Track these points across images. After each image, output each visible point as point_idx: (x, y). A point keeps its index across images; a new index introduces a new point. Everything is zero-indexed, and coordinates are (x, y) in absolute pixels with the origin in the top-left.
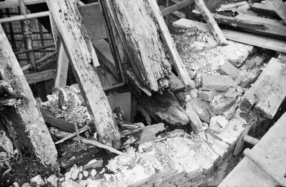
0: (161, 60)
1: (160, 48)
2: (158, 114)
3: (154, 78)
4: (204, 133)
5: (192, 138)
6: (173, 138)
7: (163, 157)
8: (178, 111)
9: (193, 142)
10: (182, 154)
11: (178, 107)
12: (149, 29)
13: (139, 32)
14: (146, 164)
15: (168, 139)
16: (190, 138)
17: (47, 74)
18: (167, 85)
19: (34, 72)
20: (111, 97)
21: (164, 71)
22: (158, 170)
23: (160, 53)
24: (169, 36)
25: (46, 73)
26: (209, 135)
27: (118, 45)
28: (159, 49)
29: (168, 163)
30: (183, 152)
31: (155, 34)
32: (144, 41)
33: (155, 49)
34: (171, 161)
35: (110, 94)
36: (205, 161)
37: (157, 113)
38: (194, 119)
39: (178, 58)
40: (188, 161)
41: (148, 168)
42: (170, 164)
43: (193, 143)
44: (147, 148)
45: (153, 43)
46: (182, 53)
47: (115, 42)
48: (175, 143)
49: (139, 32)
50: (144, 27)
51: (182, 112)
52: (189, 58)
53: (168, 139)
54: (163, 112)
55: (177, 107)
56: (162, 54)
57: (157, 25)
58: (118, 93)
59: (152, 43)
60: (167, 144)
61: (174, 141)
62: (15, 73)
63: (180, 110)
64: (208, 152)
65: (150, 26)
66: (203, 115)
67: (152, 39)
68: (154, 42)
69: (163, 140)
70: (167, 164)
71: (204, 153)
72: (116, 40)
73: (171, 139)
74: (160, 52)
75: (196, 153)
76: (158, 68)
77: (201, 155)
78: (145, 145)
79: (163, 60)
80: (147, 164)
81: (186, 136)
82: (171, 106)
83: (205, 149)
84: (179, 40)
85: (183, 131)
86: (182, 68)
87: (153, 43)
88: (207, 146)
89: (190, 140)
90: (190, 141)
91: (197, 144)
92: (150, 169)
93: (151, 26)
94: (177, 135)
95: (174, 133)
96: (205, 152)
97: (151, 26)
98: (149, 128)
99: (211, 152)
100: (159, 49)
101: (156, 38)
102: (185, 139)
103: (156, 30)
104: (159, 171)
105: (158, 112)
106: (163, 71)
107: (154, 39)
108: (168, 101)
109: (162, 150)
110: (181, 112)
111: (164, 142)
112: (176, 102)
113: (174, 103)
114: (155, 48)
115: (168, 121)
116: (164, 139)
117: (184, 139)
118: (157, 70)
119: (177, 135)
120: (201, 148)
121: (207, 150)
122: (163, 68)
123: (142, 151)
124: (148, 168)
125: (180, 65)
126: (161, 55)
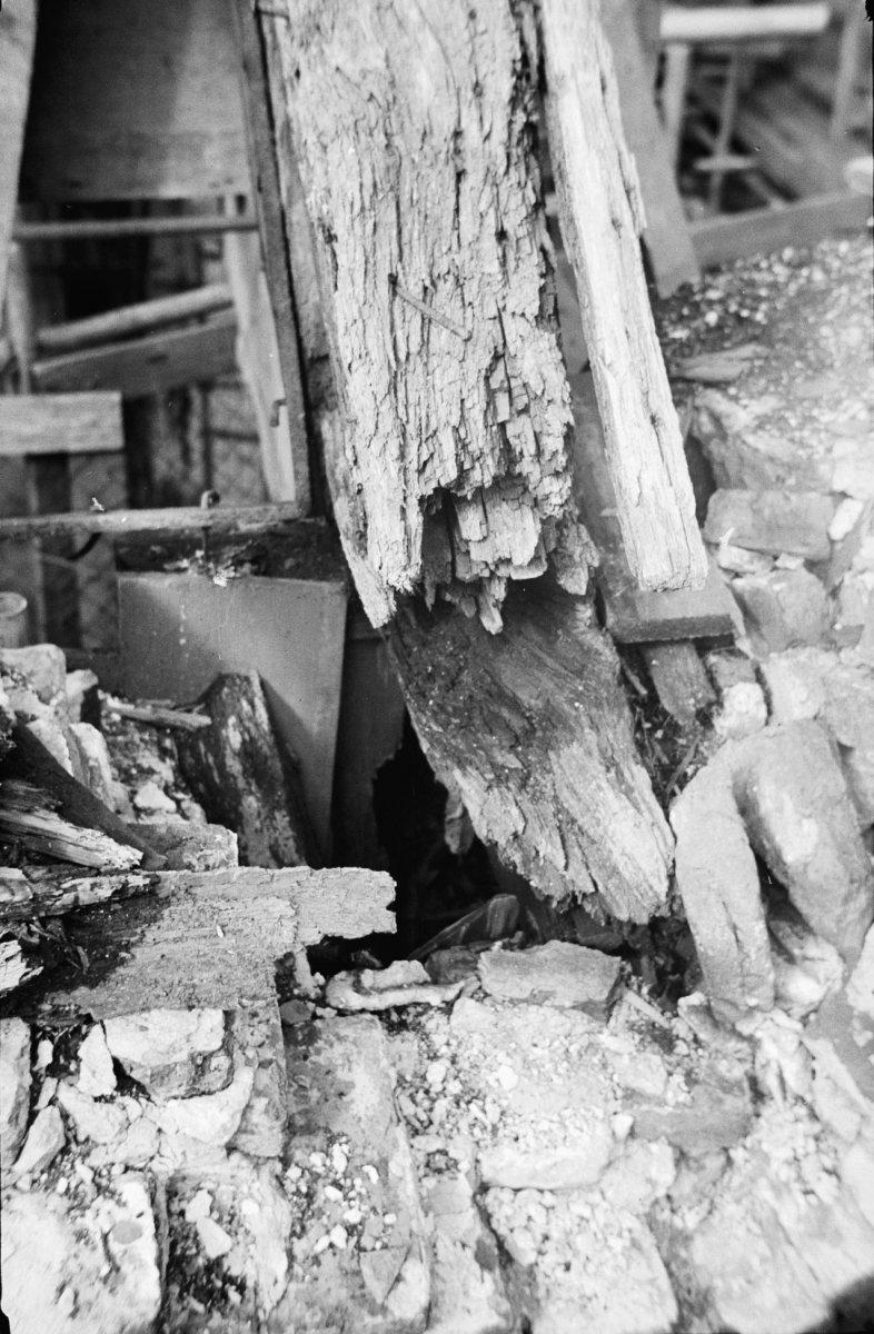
0: (494, 328)
1: (507, 227)
2: (463, 783)
3: (394, 467)
4: (799, 1026)
5: (681, 1048)
6: (508, 1013)
7: (340, 1164)
8: (611, 798)
9: (678, 1079)
10: (539, 1167)
11: (616, 765)
12: (449, 42)
13: (354, 55)
14: (110, 1204)
15: (467, 1009)
16: (666, 1041)
17: (87, 417)
18: (517, 561)
19: (17, 391)
20: (185, 587)
21: (511, 430)
22: (228, 1280)
23: (495, 267)
24: (602, 124)
25: (80, 407)
26: (835, 1058)
27: (290, 203)
28: (502, 235)
29: (351, 1230)
30: (562, 1152)
31: (489, 96)
32: (381, 139)
33: (464, 228)
34: (390, 1219)
35: (185, 563)
36: (763, 1260)
37: (457, 773)
38: (712, 898)
39: (633, 330)
40: (581, 1242)
41: (109, 1257)
42: (366, 1242)
43: (677, 1091)
44: (157, 1062)
45: (460, 175)
46: (802, 358)
47: (277, 174)
48: (518, 1058)
49: (354, 55)
50: (413, 15)
51: (638, 810)
52: (839, 402)
53: (466, 1007)
54: (500, 777)
55: (610, 764)
56: (514, 279)
57: (528, 21)
58: (256, 573)
59: (450, 173)
60: (444, 1050)
61: (510, 1034)
62: (539, 526)
63: (629, 792)
64: (801, 1199)
65: (463, 17)
66: (812, 876)
67: (457, 134)
68: (469, 165)
69: (428, 1006)
70: (339, 1236)
71: (766, 1194)
72: (282, 163)
73: (493, 1018)
74: (504, 262)
75: (689, 1180)
76: (449, 387)
77: (738, 1201)
78: (152, 1033)
79: (514, 328)
80: (121, 1215)
81: (634, 1018)
82: (569, 743)
83: (775, 1165)
84: (827, 271)
85: (606, 970)
86: (647, 423)
87: (460, 175)
88: (800, 1142)
89: (654, 1058)
90: (649, 1072)
91: (704, 1107)
92: (126, 1268)
93: (472, 15)
94: (547, 996)
95: (524, 970)
96: (779, 1189)
97: (472, 15)
98: (233, 892)
99: (828, 1200)
100: (502, 235)
101: (491, 128)
102: (616, 1040)
103: (508, 57)
104: (241, 1288)
105: (464, 775)
106: (502, 426)
107: (472, 137)
108: (560, 699)
109: (353, 1095)
110: (632, 811)
111: (430, 1026)
112: (620, 716)
113: (595, 727)
114: (462, 218)
115: (517, 858)
116: (433, 996)
117: (605, 1039)
118: (443, 412)
119: (547, 996)
120: (749, 1142)
121: (800, 1178)
122: (502, 400)
123: (108, 1083)
124: (109, 1257)
125: (633, 393)
126: (506, 283)
